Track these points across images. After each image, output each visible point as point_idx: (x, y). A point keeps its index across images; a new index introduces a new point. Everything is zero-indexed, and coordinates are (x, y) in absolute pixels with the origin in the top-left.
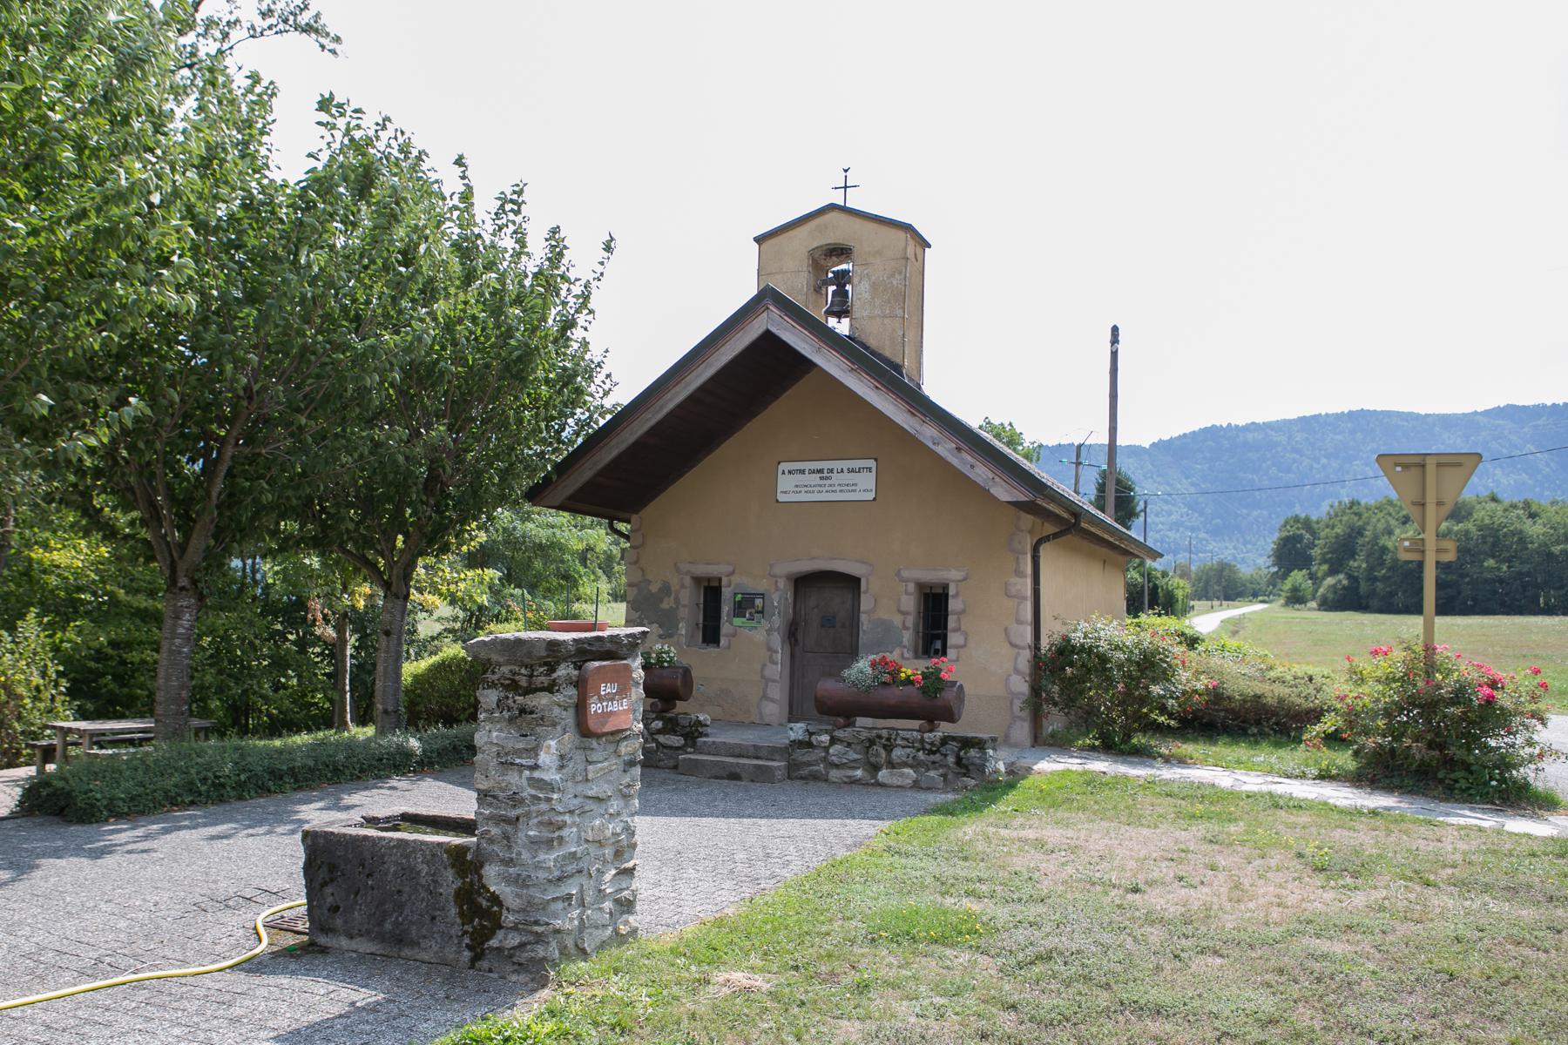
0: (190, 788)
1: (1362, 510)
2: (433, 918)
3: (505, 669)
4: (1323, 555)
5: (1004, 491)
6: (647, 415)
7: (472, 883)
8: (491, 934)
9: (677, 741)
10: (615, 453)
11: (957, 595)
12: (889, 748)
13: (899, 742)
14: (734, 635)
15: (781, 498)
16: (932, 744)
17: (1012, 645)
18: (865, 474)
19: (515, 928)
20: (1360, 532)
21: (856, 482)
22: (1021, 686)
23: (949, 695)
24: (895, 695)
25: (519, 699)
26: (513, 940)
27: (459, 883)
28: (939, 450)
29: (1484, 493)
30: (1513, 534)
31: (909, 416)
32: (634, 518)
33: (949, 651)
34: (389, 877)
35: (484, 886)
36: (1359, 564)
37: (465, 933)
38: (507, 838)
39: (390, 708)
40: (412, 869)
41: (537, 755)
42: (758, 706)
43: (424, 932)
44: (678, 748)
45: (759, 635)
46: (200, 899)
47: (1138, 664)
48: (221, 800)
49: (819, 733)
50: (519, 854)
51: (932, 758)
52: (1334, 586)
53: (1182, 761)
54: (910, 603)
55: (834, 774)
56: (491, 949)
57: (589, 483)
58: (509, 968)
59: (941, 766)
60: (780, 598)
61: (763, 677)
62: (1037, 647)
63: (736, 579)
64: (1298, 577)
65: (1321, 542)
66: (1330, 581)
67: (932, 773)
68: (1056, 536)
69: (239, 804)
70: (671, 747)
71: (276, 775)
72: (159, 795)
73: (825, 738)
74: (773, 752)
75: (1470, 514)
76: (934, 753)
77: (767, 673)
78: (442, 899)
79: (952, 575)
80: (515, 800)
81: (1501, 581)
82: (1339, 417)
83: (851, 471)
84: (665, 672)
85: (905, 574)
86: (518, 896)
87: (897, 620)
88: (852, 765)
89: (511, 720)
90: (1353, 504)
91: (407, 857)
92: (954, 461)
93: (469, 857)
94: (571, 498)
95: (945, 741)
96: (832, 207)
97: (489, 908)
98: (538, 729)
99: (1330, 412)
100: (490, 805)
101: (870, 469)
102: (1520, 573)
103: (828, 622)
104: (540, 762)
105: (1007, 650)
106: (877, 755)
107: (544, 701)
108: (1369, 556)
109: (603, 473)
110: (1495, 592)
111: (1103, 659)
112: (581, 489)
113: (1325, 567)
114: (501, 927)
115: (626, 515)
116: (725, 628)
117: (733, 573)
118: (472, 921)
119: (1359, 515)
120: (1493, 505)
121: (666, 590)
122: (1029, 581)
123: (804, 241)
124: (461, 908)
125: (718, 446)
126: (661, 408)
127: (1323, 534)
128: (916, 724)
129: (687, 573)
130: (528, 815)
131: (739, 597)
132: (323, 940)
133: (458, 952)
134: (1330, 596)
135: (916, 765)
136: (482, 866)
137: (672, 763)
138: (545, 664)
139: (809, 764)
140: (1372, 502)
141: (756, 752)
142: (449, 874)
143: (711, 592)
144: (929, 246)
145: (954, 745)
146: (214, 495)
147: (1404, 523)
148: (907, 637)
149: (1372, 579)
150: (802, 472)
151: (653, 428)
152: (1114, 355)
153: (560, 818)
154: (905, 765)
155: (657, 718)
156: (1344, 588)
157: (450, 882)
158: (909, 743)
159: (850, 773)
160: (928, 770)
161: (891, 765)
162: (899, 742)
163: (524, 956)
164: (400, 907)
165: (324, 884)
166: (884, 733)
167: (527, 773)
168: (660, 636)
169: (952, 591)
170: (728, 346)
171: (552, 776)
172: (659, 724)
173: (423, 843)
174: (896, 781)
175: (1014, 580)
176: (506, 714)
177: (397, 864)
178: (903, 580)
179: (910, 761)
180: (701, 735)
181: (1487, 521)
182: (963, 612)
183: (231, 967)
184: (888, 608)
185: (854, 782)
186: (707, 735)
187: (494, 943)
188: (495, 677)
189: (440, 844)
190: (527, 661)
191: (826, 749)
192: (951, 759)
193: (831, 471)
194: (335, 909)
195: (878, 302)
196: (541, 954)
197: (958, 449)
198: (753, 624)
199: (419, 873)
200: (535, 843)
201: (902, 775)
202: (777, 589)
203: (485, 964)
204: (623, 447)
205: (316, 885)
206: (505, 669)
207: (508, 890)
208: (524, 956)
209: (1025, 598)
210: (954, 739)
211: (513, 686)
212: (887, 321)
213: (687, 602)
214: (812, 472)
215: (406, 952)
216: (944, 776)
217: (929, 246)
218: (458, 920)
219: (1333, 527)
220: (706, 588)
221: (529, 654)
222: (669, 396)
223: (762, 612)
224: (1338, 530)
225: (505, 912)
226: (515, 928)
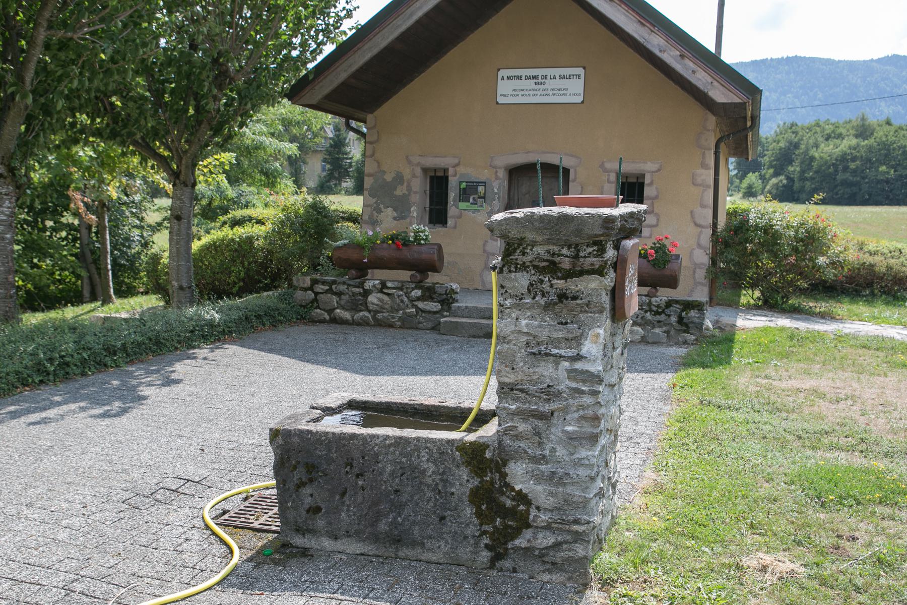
0: (39, 368)
1: (798, 129)
2: (442, 518)
3: (540, 250)
4: (771, 162)
6: (398, 22)
7: (492, 483)
8: (516, 532)
9: (434, 306)
10: (368, 56)
11: (651, 184)
15: (501, 100)
16: (658, 306)
17: (696, 225)
18: (574, 81)
19: (548, 527)
20: (797, 146)
21: (566, 86)
25: (560, 283)
26: (545, 540)
27: (476, 482)
29: (883, 118)
30: (900, 148)
32: (370, 117)
34: (385, 477)
35: (507, 485)
36: (794, 169)
37: (484, 533)
38: (538, 434)
39: (185, 285)
40: (414, 468)
41: (579, 345)
42: (481, 275)
43: (430, 532)
46: (126, 495)
47: (802, 240)
48: (67, 377)
50: (553, 450)
51: (658, 318)
52: (777, 184)
56: (517, 549)
57: (343, 84)
58: (538, 567)
59: (665, 325)
61: (485, 251)
62: (715, 225)
63: (461, 170)
64: (752, 178)
65: (770, 153)
66: (774, 181)
67: (657, 330)
69: (83, 381)
70: (429, 312)
71: (111, 351)
72: (12, 378)
75: (872, 134)
77: (489, 248)
78: (455, 499)
79: (647, 167)
80: (550, 393)
81: (887, 181)
82: (780, 61)
83: (562, 77)
84: (423, 249)
86: (551, 494)
89: (547, 307)
90: (792, 125)
91: (408, 455)
93: (488, 455)
94: (328, 97)
95: (669, 304)
97: (514, 508)
98: (582, 316)
99: (774, 57)
100: (517, 399)
101: (579, 75)
102: (901, 176)
104: (583, 352)
105: (692, 230)
107: (593, 285)
108: (802, 163)
109: (356, 75)
110: (884, 190)
111: (776, 236)
112: (335, 91)
113: (771, 171)
114: (528, 526)
115: (361, 115)
116: (452, 211)
117: (458, 165)
118: (493, 521)
119: (796, 133)
120: (888, 127)
122: (712, 172)
124: (479, 508)
125: (445, 53)
126: (411, 15)
127: (771, 147)
129: (418, 164)
130: (565, 410)
131: (464, 185)
132: (299, 541)
133: (476, 553)
134: (774, 191)
136: (505, 464)
137: (430, 325)
138: (595, 243)
140: (806, 124)
142: (464, 473)
143: (438, 183)
145: (677, 308)
146: (28, 80)
147: (827, 139)
149: (803, 179)
150: (520, 78)
151: (403, 35)
155: (416, 288)
156: (784, 186)
157: (464, 481)
160: (654, 327)
163: (559, 556)
164: (399, 507)
165: (301, 485)
167: (566, 364)
168: (395, 218)
169: (647, 180)
171: (596, 367)
172: (418, 293)
173: (427, 440)
175: (701, 171)
176: (542, 301)
177: (394, 463)
178: (606, 171)
181: (884, 139)
182: (657, 197)
183: (218, 583)
186: (457, 301)
187: (521, 542)
188: (525, 259)
189: (450, 442)
190: (574, 239)
192: (674, 319)
193: (545, 77)
194: (315, 510)
196: (581, 552)
197: (682, 56)
198: (476, 207)
199: (423, 472)
200: (573, 440)
202: (497, 178)
203: (507, 564)
204: (375, 51)
205: (291, 486)
206: (540, 250)
207: (539, 488)
208: (559, 556)
210: (677, 302)
211: (552, 268)
213: (418, 192)
214: (528, 78)
215: (405, 552)
216: (667, 332)
218: (475, 520)
219: (778, 142)
220: (432, 178)
221: (578, 232)
223: (484, 198)
224: (782, 144)
225: (533, 512)
226: (548, 527)
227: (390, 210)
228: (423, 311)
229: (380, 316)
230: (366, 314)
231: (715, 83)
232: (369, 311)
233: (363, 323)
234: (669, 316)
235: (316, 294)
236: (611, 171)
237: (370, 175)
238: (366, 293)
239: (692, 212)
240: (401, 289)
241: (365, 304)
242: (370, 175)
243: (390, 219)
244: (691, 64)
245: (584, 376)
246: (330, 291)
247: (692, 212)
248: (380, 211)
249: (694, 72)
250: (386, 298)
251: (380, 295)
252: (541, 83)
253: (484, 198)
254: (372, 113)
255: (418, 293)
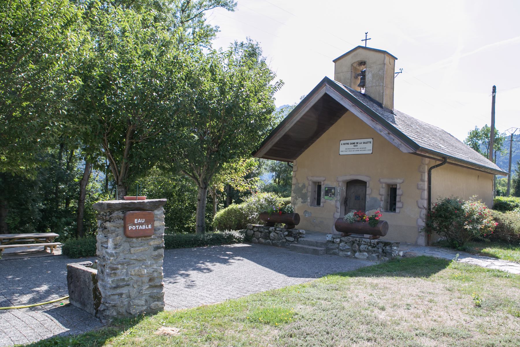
5: (405, 149)
9: (291, 239)
10: (278, 139)
11: (400, 188)
12: (359, 245)
13: (363, 243)
14: (325, 202)
15: (341, 153)
16: (374, 244)
17: (419, 207)
21: (366, 147)
22: (422, 223)
23: (380, 227)
24: (361, 225)
28: (382, 133)
31: (372, 122)
33: (397, 209)
44: (292, 242)
45: (333, 202)
49: (337, 238)
51: (374, 249)
53: (495, 257)
54: (384, 191)
55: (341, 253)
57: (271, 149)
60: (340, 189)
61: (334, 217)
62: (430, 209)
63: (326, 182)
67: (374, 255)
68: (437, 166)
73: (338, 240)
74: (322, 244)
76: (374, 247)
79: (399, 181)
83: (364, 143)
85: (382, 180)
87: (379, 198)
88: (347, 250)
92: (387, 138)
94: (265, 154)
96: (359, 47)
103: (357, 198)
106: (355, 247)
116: (322, 200)
121: (304, 186)
122: (426, 184)
123: (349, 60)
126: (292, 122)
128: (368, 236)
131: (327, 189)
135: (368, 251)
139: (333, 249)
141: (316, 244)
144: (397, 59)
148: (382, 204)
150: (348, 144)
152: (494, 98)
153: (115, 266)
154: (364, 251)
158: (366, 243)
159: (346, 253)
160: (372, 253)
161: (360, 251)
162: (363, 243)
166: (358, 239)
170: (313, 99)
174: (361, 257)
175: (421, 183)
178: (381, 183)
179: (366, 250)
180: (301, 237)
182: (402, 195)
184: (376, 193)
185: (347, 256)
191: (339, 244)
192: (380, 250)
193: (357, 143)
195: (374, 81)
198: (331, 198)
201: (363, 255)
204: (281, 137)
209: (424, 190)
210: (381, 242)
212: (377, 88)
213: (310, 190)
214: (351, 144)
216: (378, 256)
217: (397, 59)
220: (391, 188)
222: (295, 118)
223: (334, 194)
227: (300, 199)
228: (288, 241)
229: (274, 242)
230: (269, 240)
231: (402, 144)
232: (271, 240)
233: (268, 244)
234: (378, 248)
235: (254, 231)
236: (383, 183)
237: (294, 184)
238: (270, 232)
239: (417, 202)
240: (281, 231)
241: (269, 237)
242: (294, 184)
243: (300, 203)
244: (392, 137)
245: (11, 241)
246: (258, 231)
247: (417, 202)
248: (297, 199)
249: (394, 140)
250: (276, 235)
251: (274, 233)
252: (356, 146)
253: (334, 194)
254: (295, 159)
255: (286, 233)
